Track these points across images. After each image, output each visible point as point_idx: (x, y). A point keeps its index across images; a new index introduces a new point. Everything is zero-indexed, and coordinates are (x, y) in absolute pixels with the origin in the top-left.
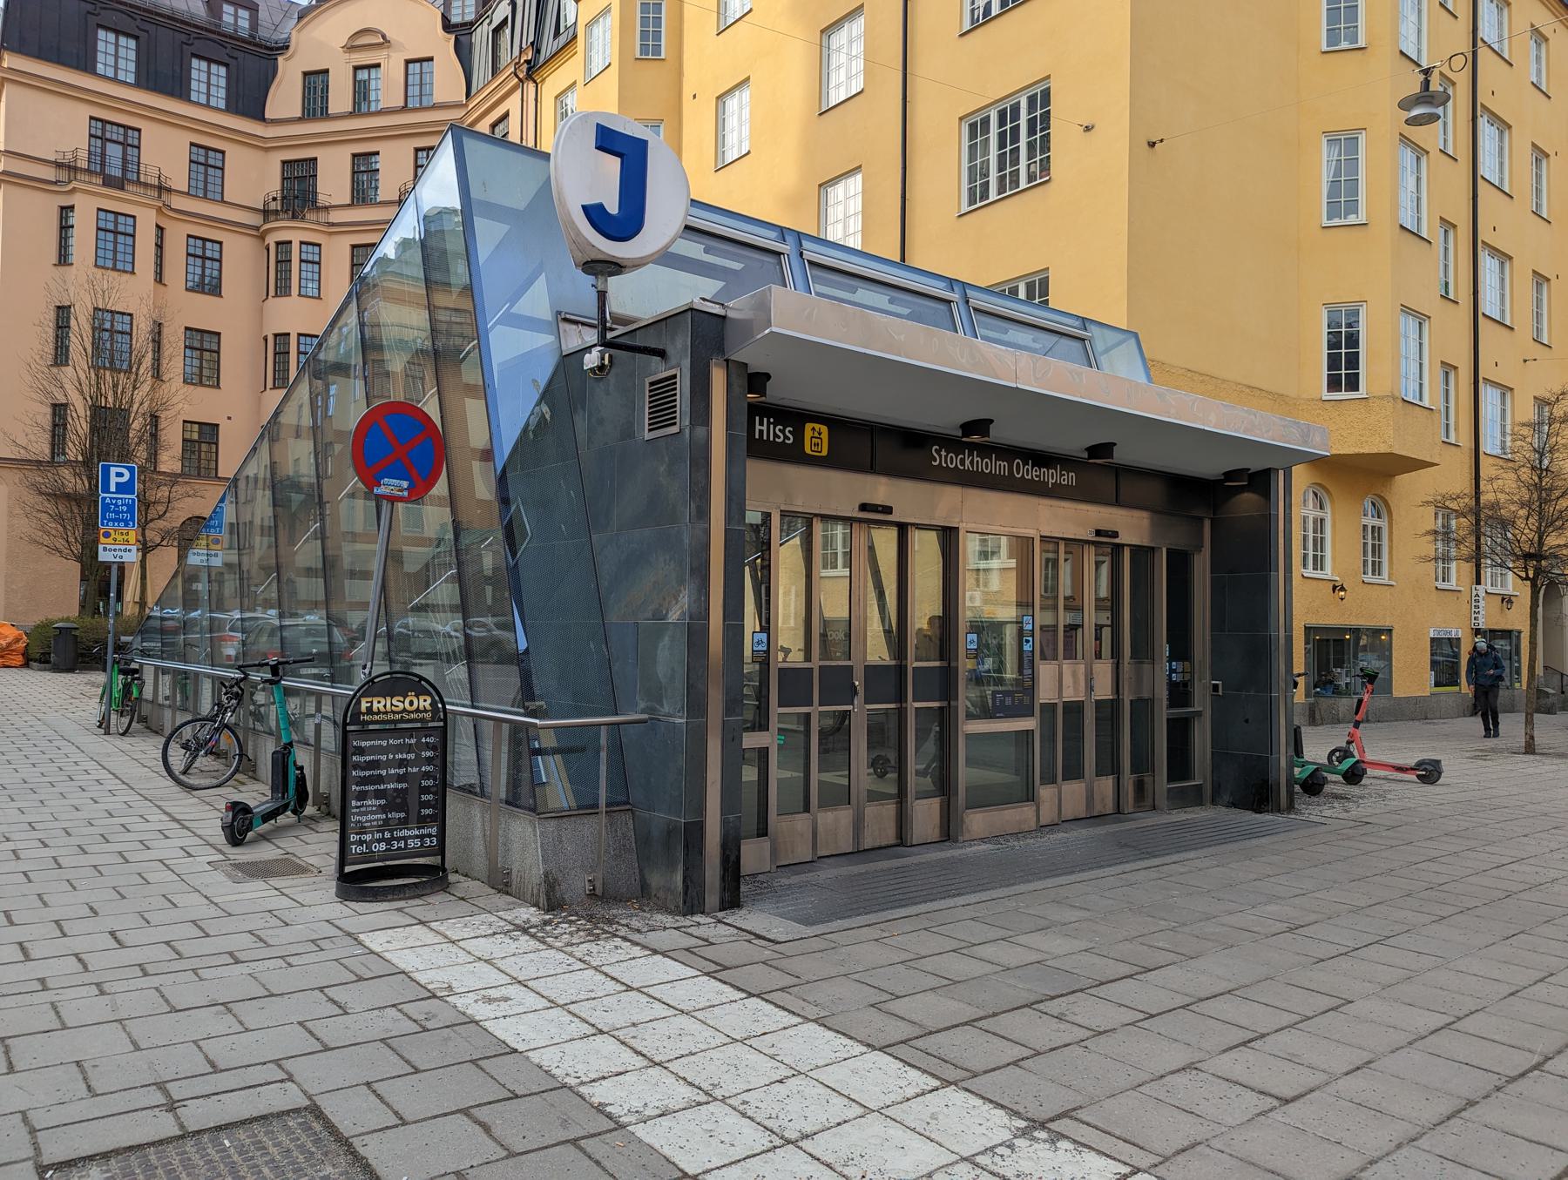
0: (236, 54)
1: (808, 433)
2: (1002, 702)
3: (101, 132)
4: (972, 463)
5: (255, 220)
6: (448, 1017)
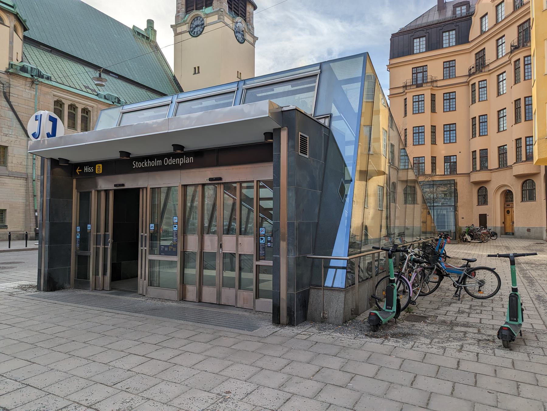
0: (458, 24)
1: (97, 167)
2: (164, 249)
4: (147, 164)
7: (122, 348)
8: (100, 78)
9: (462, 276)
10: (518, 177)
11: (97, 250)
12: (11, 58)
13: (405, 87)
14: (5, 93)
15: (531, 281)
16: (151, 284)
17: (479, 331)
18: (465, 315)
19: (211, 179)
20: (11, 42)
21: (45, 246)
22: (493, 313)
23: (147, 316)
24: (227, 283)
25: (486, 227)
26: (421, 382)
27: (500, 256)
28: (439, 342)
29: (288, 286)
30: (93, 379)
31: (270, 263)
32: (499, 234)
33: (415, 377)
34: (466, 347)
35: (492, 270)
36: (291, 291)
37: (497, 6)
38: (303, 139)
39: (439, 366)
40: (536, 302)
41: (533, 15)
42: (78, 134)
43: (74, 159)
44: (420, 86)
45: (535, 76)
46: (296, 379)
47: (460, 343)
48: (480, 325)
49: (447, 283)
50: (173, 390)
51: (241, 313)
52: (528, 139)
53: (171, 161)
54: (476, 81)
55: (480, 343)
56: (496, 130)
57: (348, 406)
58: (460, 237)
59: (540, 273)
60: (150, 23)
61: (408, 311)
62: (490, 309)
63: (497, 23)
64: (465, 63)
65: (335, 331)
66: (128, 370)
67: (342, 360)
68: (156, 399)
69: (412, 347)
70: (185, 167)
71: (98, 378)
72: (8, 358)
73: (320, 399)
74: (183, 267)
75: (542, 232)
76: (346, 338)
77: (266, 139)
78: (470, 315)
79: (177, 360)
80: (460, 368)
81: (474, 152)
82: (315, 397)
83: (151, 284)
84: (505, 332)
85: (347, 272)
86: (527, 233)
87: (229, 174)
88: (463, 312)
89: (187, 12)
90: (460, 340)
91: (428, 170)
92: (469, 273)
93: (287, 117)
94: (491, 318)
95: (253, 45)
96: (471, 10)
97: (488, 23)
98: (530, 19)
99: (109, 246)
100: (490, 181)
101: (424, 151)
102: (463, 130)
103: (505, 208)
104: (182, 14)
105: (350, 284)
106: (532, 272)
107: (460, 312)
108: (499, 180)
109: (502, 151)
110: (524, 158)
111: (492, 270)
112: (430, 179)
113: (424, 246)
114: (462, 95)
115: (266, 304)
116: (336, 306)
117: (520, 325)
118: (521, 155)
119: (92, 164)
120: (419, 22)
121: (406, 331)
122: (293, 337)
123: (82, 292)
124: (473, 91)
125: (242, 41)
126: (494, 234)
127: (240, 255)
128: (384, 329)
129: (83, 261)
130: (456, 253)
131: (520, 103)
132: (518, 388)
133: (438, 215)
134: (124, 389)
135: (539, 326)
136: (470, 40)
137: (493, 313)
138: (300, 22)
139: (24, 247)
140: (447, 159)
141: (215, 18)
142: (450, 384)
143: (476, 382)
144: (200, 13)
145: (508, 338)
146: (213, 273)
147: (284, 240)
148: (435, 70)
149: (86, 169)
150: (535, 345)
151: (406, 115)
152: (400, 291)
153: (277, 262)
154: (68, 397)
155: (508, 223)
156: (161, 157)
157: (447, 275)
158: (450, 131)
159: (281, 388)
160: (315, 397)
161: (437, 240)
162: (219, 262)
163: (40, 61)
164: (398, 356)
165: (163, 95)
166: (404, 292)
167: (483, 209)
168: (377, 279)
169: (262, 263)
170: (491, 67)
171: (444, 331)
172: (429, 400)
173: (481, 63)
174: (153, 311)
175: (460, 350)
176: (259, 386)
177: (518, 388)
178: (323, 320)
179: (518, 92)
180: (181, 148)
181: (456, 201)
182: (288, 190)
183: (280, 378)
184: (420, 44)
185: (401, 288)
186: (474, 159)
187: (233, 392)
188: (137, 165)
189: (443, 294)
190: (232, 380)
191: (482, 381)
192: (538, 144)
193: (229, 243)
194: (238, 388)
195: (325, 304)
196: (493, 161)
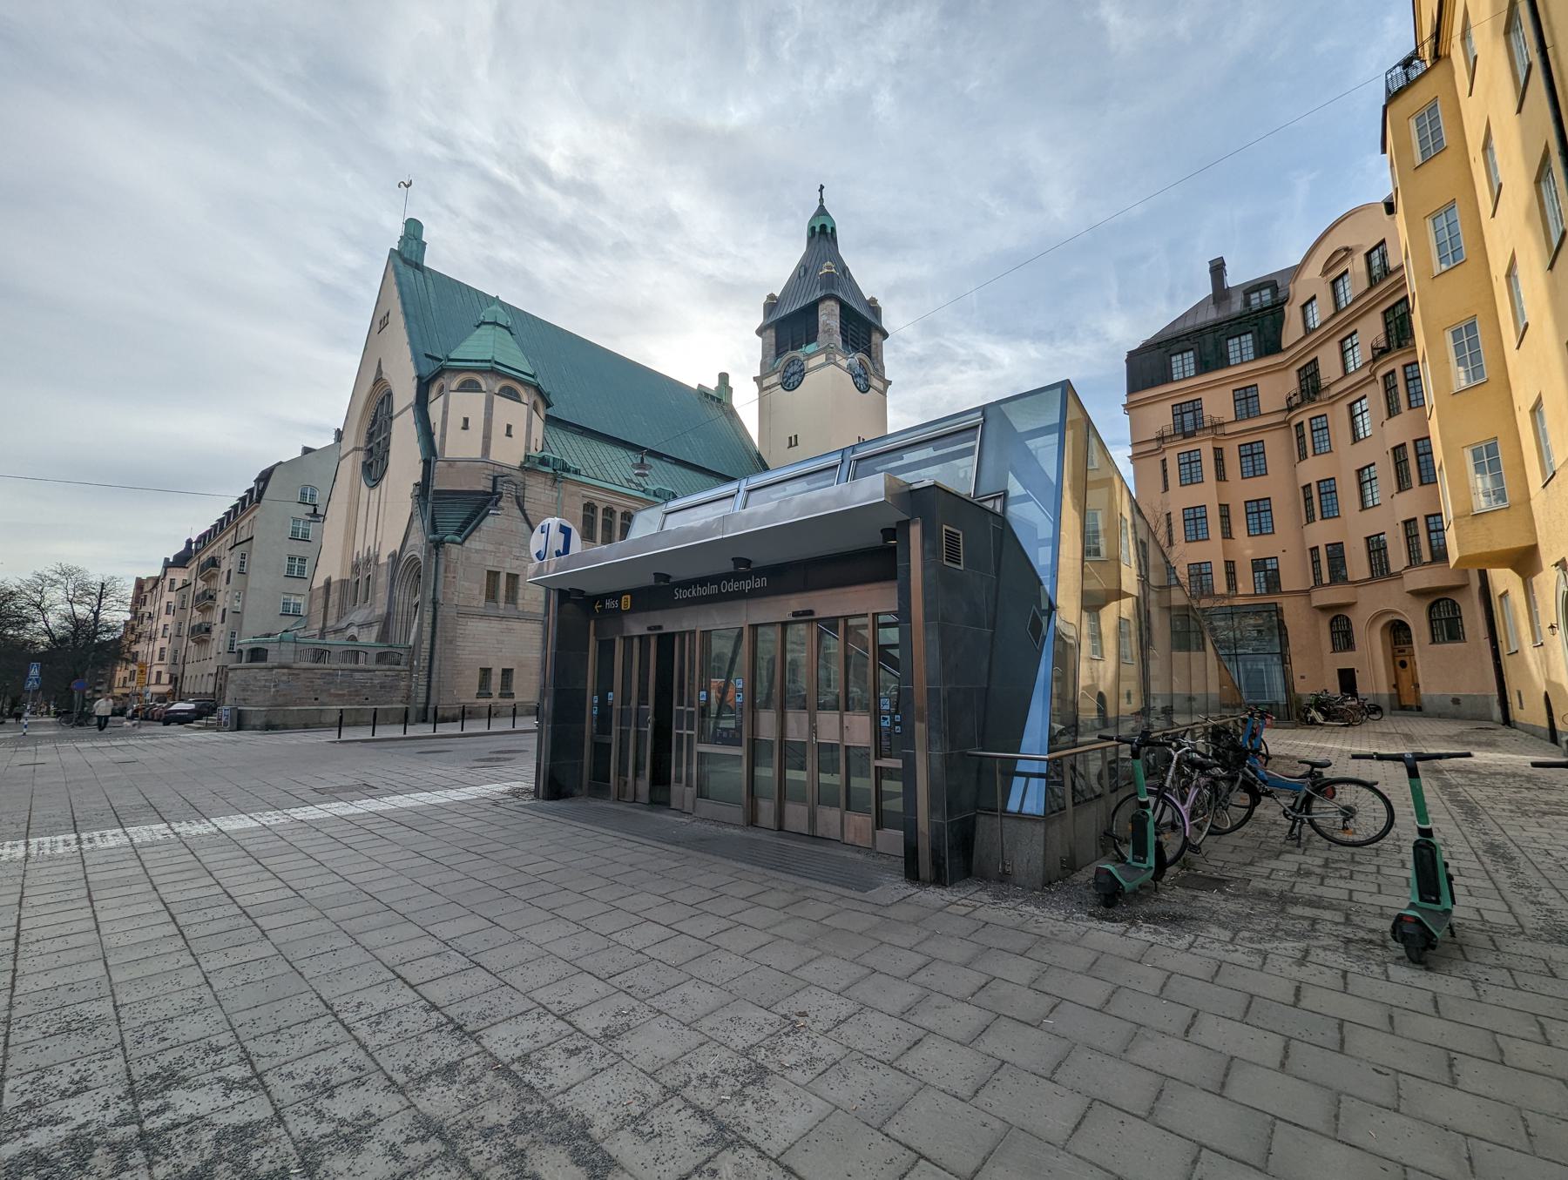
7: (635, 909)
8: (641, 465)
9: (1302, 795)
10: (1418, 594)
11: (624, 734)
12: (528, 448)
13: (1161, 438)
14: (517, 498)
15: (1471, 811)
16: (701, 794)
17: (1347, 918)
18: (1314, 880)
19: (795, 614)
20: (529, 426)
21: (547, 726)
22: (1381, 880)
23: (690, 852)
24: (825, 797)
25: (1354, 695)
26: (1212, 1031)
27: (1381, 758)
28: (1251, 940)
29: (932, 809)
30: (578, 963)
31: (897, 763)
32: (1386, 710)
33: (1195, 1016)
34: (1318, 955)
35: (1370, 786)
36: (937, 819)
37: (1334, 282)
38: (952, 538)
39: (1252, 996)
40: (1484, 859)
41: (1412, 287)
42: (600, 548)
43: (592, 588)
44: (1193, 434)
45: (1430, 397)
46: (936, 999)
47: (1302, 945)
48: (1350, 904)
49: (1269, 810)
50: (702, 997)
51: (849, 855)
52: (1431, 520)
53: (732, 586)
54: (1305, 418)
55: (1351, 947)
56: (1358, 506)
57: (1041, 1072)
58: (1297, 714)
59: (1492, 792)
60: (724, 377)
61: (1186, 865)
62: (1373, 869)
63: (1338, 311)
64: (1276, 388)
65: (1027, 902)
66: (639, 952)
67: (1036, 965)
68: (673, 1013)
69: (1191, 946)
70: (754, 594)
71: (586, 963)
72: (463, 911)
73: (982, 1047)
74: (753, 764)
75: (1488, 705)
76: (1046, 918)
77: (885, 539)
78: (1327, 881)
79: (723, 940)
80: (1303, 1004)
81: (1315, 550)
82: (970, 1042)
83: (701, 794)
84: (1408, 929)
85: (1048, 784)
86: (1453, 708)
87: (828, 603)
88: (1308, 874)
89: (778, 355)
90: (1301, 936)
91: (1220, 586)
92: (1318, 790)
93: (922, 503)
94: (1375, 889)
95: (884, 393)
96: (1281, 295)
97: (1317, 316)
98: (1406, 297)
99: (649, 729)
100: (1353, 604)
101: (1212, 551)
102: (1284, 513)
103: (1394, 656)
104: (770, 360)
105: (1054, 810)
106: (1471, 790)
107: (1302, 873)
108: (1372, 604)
109: (1376, 548)
110: (1426, 557)
111: (1370, 786)
112: (1227, 602)
113: (1217, 734)
114: (1276, 446)
115: (892, 839)
116: (1029, 851)
117: (1448, 912)
118: (1419, 550)
119: (617, 595)
120: (1179, 327)
121: (1179, 909)
122: (940, 910)
123: (600, 804)
124: (1301, 437)
125: (865, 389)
126: (1376, 709)
127: (847, 748)
128: (1128, 904)
129: (602, 750)
130: (1287, 745)
131: (1405, 452)
132: (1451, 1066)
133: (1246, 671)
134: (623, 987)
135: (1496, 914)
136: (1284, 346)
137: (1381, 880)
138: (962, 351)
139: (401, 735)
140: (1258, 565)
141: (822, 359)
142: (1278, 1042)
143: (1342, 1041)
144: (798, 354)
145: (1421, 941)
146: (801, 776)
147: (921, 721)
148: (1218, 404)
149: (609, 604)
150: (1491, 959)
151: (1166, 489)
152: (1165, 825)
153: (910, 763)
154: (532, 995)
155: (1406, 687)
156: (716, 579)
157: (1268, 794)
158: (1259, 512)
159: (904, 1015)
160: (970, 1042)
161: (1245, 721)
162: (811, 760)
163: (572, 450)
164: (1158, 964)
165: (730, 479)
166: (1173, 826)
167: (1345, 660)
168: (1114, 800)
169: (885, 763)
170: (1334, 391)
171: (1264, 915)
172: (1226, 1075)
173: (1311, 385)
174: (701, 844)
175: (1302, 961)
176: (863, 1007)
177: (1451, 1066)
178: (1004, 878)
179: (1399, 430)
180: (748, 562)
181: (1284, 643)
182: (926, 628)
183: (903, 994)
184: (1183, 363)
185: (1167, 817)
186: (1316, 562)
187: (812, 1016)
188: (680, 594)
189: (1263, 833)
190: (814, 990)
191: (1359, 1041)
192: (1456, 528)
193: (828, 727)
194: (823, 1006)
195: (1007, 847)
196: (1358, 566)
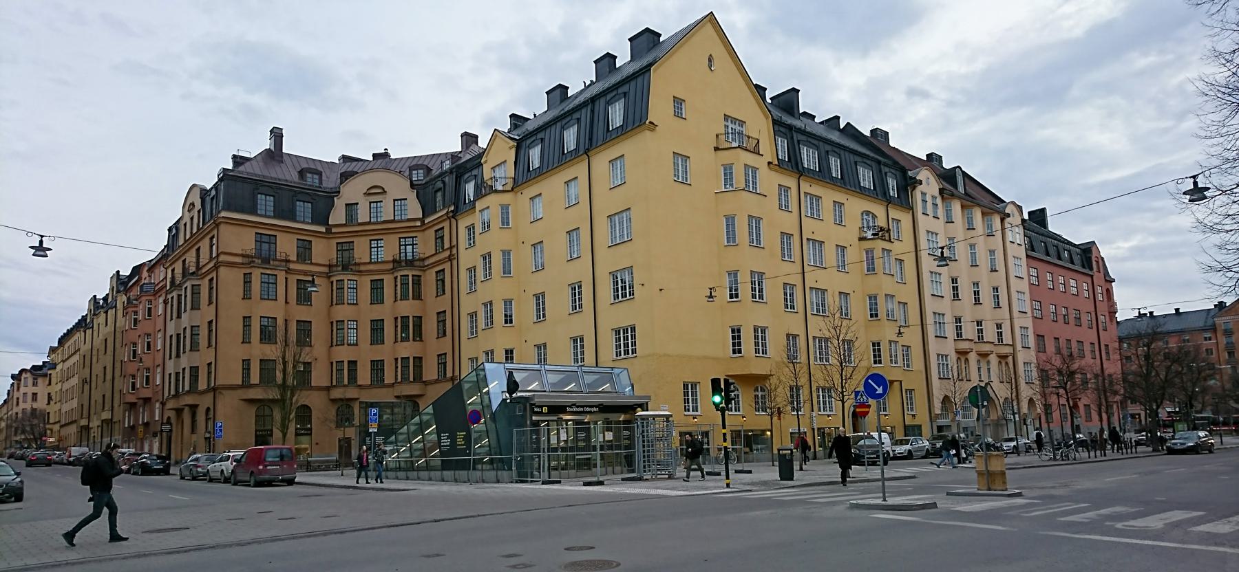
3: (259, 238)
5: (326, 270)
6: (213, 192)
